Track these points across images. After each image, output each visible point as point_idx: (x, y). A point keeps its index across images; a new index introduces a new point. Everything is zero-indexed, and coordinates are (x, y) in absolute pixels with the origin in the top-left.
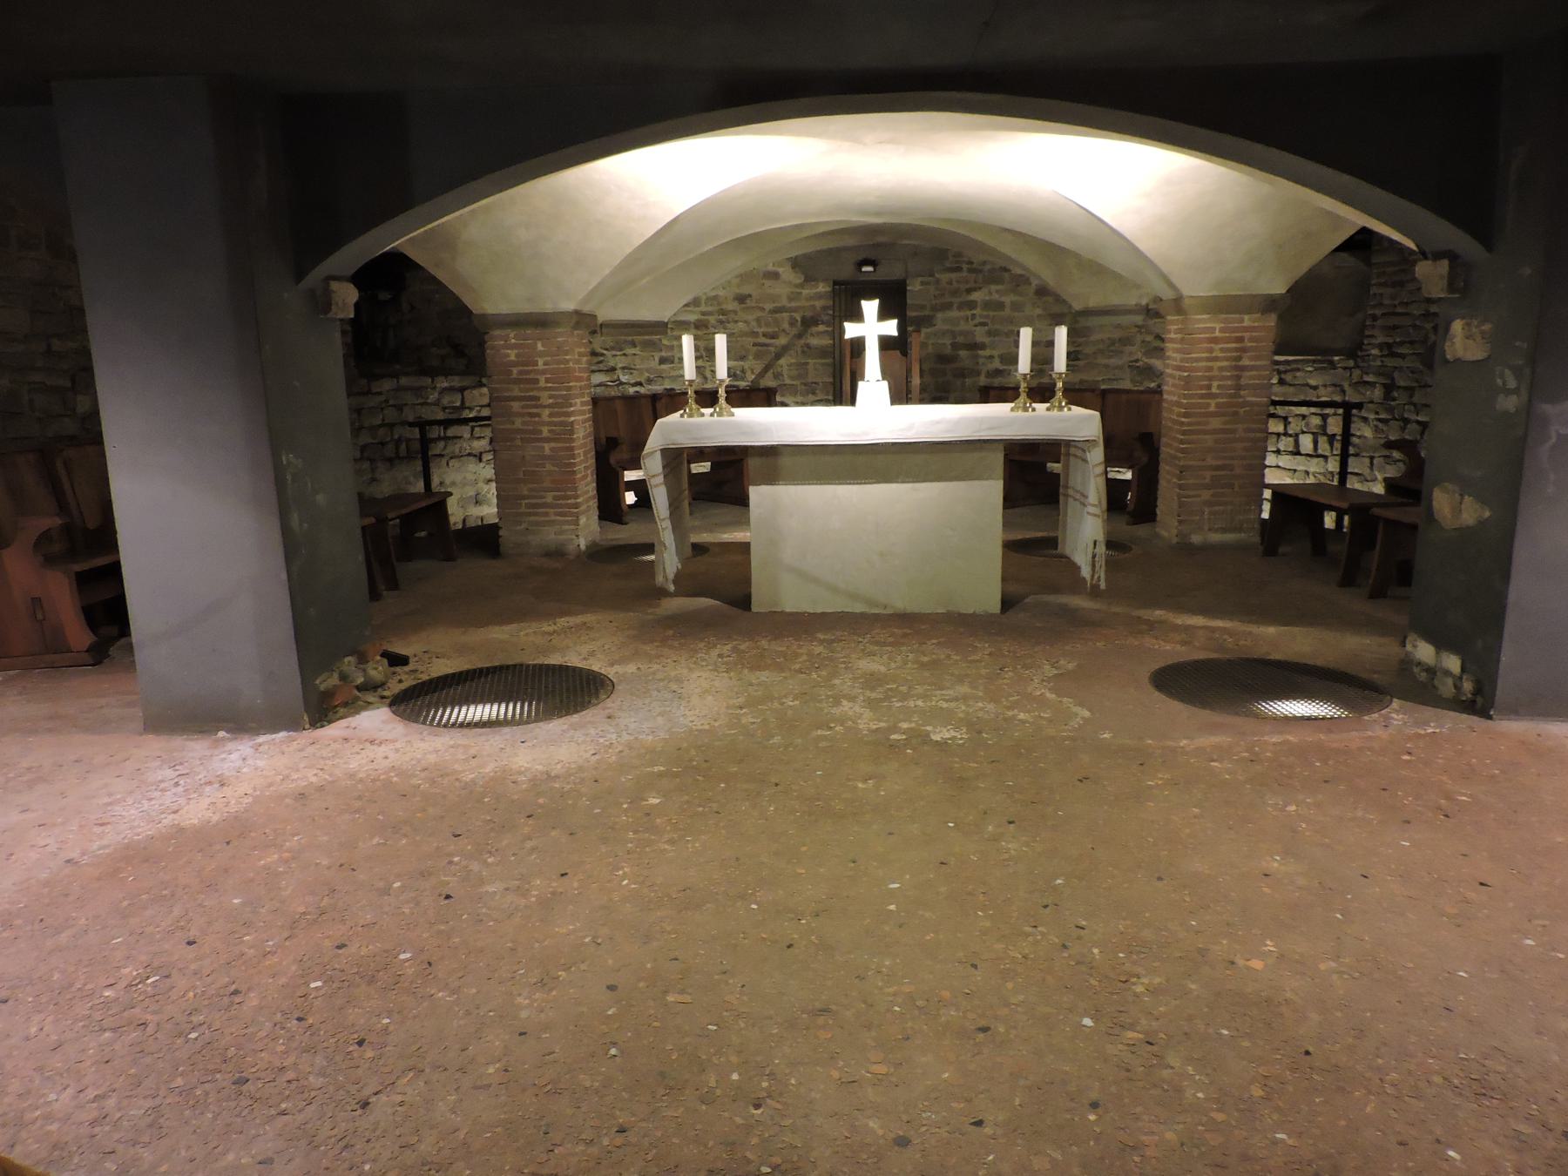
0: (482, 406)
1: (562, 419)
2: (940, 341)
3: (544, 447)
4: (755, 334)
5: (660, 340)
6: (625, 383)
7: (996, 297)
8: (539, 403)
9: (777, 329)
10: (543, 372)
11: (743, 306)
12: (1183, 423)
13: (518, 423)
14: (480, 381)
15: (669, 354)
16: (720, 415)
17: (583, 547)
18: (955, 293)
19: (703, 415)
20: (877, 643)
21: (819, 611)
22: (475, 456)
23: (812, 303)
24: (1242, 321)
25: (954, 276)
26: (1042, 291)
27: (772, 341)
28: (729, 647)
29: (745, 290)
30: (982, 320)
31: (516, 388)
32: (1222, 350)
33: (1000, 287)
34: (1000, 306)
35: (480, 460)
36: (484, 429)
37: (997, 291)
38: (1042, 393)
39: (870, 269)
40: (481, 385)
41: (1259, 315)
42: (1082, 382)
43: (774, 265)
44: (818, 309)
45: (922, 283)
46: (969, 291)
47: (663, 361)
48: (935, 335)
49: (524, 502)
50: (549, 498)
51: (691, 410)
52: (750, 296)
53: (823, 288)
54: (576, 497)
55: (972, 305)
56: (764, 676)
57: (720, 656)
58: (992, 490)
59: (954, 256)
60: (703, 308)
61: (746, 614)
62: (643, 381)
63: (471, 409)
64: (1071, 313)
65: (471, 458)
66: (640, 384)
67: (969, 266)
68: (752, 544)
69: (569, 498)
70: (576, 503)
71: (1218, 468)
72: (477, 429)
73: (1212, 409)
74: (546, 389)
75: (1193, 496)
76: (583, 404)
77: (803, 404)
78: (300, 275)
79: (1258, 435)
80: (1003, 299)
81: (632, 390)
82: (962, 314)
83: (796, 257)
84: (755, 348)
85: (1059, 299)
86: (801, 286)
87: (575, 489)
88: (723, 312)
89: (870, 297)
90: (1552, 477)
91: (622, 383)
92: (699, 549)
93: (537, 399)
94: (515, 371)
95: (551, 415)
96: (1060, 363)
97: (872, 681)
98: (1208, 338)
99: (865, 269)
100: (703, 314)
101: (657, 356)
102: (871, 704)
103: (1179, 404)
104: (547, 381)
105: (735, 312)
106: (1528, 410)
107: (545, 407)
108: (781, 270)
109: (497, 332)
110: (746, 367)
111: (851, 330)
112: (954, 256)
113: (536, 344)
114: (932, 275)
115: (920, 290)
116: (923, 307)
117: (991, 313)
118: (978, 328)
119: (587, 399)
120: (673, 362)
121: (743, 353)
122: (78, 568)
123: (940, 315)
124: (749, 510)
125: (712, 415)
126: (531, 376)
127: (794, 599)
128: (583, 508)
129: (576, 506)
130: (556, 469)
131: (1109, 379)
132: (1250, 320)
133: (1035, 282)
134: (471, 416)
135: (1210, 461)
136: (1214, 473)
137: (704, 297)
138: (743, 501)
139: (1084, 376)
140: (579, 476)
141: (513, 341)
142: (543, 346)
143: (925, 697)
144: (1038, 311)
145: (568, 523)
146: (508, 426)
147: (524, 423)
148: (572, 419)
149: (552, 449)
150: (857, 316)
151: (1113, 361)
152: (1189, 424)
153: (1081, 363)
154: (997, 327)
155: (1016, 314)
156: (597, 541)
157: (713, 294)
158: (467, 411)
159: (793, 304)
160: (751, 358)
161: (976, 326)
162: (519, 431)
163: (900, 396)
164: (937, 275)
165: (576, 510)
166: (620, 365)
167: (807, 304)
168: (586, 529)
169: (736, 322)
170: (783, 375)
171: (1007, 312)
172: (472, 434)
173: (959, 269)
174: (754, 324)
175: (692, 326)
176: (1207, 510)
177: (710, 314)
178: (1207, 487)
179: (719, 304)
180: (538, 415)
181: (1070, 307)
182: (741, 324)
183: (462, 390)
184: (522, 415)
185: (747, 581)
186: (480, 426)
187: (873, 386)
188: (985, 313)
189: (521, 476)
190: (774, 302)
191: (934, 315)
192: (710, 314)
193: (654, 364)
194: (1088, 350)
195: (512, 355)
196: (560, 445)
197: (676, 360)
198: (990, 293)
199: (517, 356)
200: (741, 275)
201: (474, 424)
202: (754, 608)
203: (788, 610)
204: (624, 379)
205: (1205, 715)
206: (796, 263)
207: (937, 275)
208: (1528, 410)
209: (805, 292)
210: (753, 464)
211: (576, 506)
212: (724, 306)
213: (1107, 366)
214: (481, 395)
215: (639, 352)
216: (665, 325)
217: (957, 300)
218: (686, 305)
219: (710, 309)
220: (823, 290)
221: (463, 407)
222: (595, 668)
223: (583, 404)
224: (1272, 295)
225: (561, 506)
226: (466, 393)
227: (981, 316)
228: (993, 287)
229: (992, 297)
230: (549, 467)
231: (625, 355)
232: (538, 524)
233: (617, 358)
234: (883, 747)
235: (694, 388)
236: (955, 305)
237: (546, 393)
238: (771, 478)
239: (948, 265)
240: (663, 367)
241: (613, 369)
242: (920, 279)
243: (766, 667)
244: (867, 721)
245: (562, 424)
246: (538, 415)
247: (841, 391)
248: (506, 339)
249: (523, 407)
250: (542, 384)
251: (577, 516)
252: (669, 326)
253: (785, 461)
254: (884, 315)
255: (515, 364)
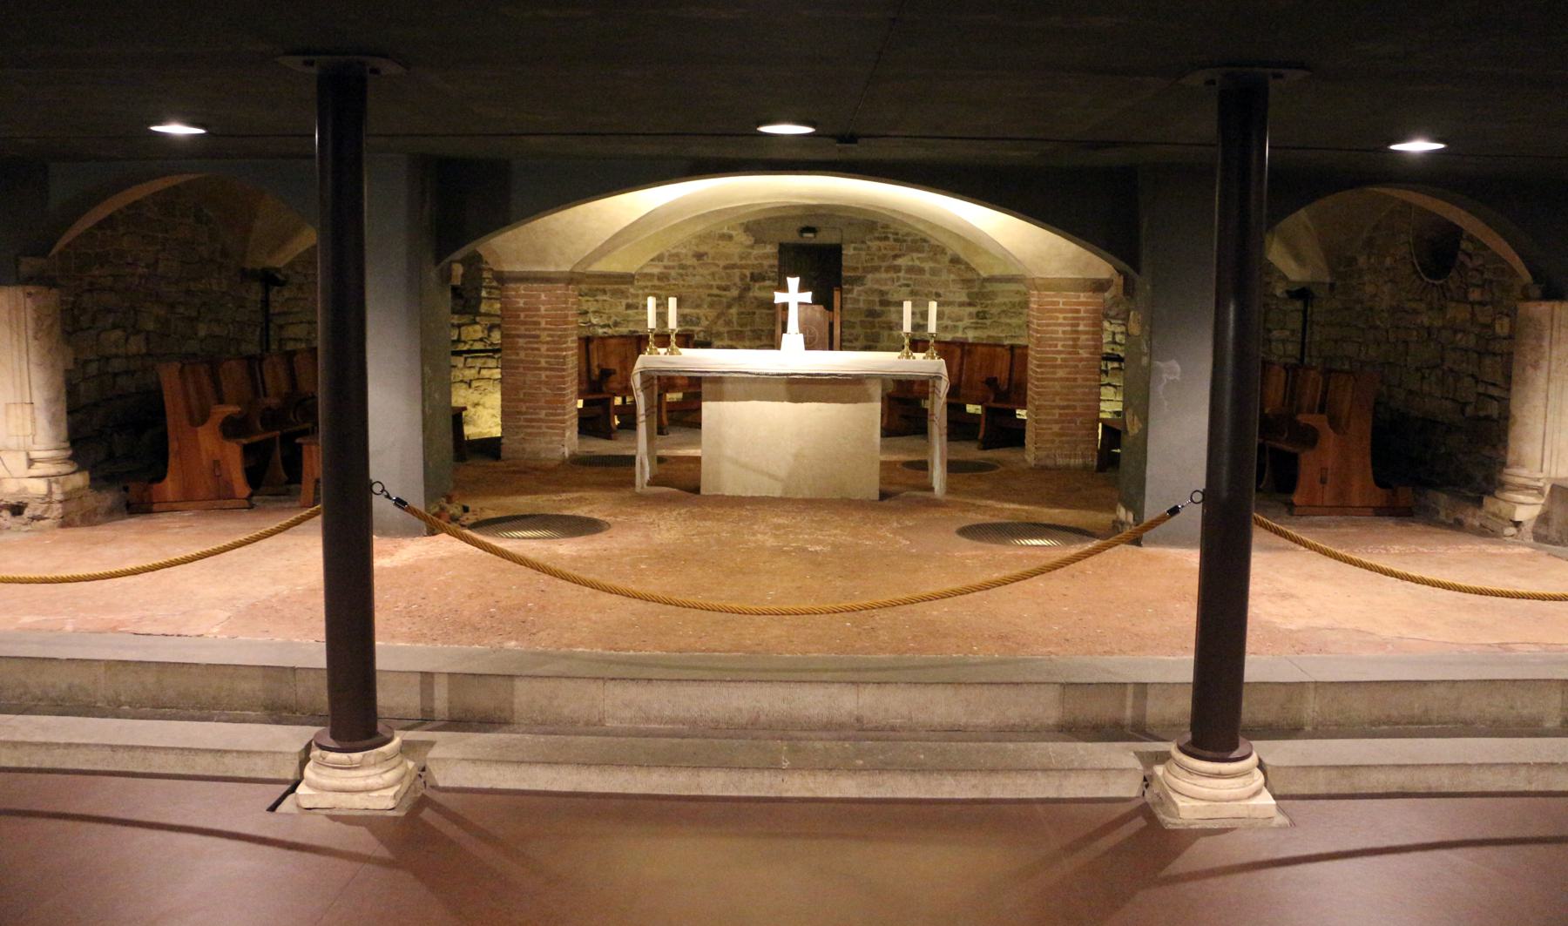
0: (474, 341)
1: (558, 353)
2: (871, 298)
3: (540, 375)
4: (711, 287)
5: (628, 289)
6: (595, 325)
7: (917, 263)
8: (539, 340)
9: (729, 283)
10: (543, 317)
11: (701, 262)
12: (1037, 372)
13: (522, 355)
14: (474, 320)
15: (635, 301)
16: (672, 354)
17: (567, 455)
18: (883, 258)
19: (659, 354)
20: (785, 511)
21: (749, 494)
22: (466, 382)
23: (760, 261)
24: (1079, 297)
25: (882, 244)
26: (955, 260)
27: (724, 293)
28: (685, 510)
29: (703, 249)
30: (905, 282)
31: (523, 328)
32: (1065, 318)
33: (920, 255)
34: (921, 271)
35: (470, 386)
36: (476, 360)
37: (918, 258)
38: (918, 345)
39: (811, 235)
40: (476, 323)
41: (1091, 294)
42: (989, 337)
43: (728, 229)
44: (766, 268)
45: (855, 249)
46: (895, 257)
47: (629, 307)
48: (866, 293)
49: (522, 417)
50: (542, 414)
51: (651, 349)
52: (706, 254)
53: (771, 249)
54: (565, 415)
55: (897, 269)
56: (708, 523)
57: (679, 514)
58: (871, 412)
59: (882, 228)
60: (666, 262)
61: (697, 496)
62: (611, 323)
63: (465, 342)
64: (978, 279)
65: (462, 384)
66: (609, 326)
67: (895, 237)
68: (703, 460)
69: (559, 415)
70: (564, 420)
71: (1064, 408)
72: (469, 360)
73: (1059, 362)
74: (545, 329)
75: (1046, 429)
76: (573, 342)
77: (751, 348)
78: (437, 263)
79: (1093, 383)
80: (923, 265)
81: (600, 331)
82: (889, 275)
83: (748, 222)
84: (709, 299)
85: (969, 268)
86: (752, 247)
87: (564, 408)
88: (683, 267)
89: (793, 275)
90: (1166, 403)
91: (593, 325)
92: (661, 460)
93: (537, 337)
94: (522, 315)
95: (548, 350)
96: (932, 326)
97: (778, 527)
98: (1071, 309)
99: (806, 235)
100: (665, 267)
101: (624, 302)
102: (776, 536)
103: (1036, 358)
104: (547, 323)
105: (694, 268)
106: (1150, 364)
107: (544, 343)
108: (734, 233)
109: (512, 285)
110: (701, 314)
111: (779, 297)
112: (882, 228)
113: (540, 295)
114: (863, 242)
115: (853, 255)
116: (855, 269)
117: (913, 276)
118: (903, 288)
119: (575, 338)
120: (637, 308)
121: (699, 302)
122: (245, 441)
123: (870, 276)
124: (700, 434)
125: (666, 354)
126: (535, 319)
127: (729, 490)
128: (569, 423)
129: (563, 422)
130: (550, 392)
131: (1012, 336)
132: (1084, 296)
133: (949, 252)
134: (465, 348)
135: (1058, 402)
136: (1062, 411)
137: (667, 254)
138: (697, 425)
139: (992, 333)
140: (567, 398)
141: (523, 292)
142: (546, 296)
143: (810, 534)
144: (952, 276)
145: (557, 435)
146: (513, 357)
147: (527, 355)
148: (564, 353)
149: (547, 377)
150: (783, 288)
151: (1014, 321)
152: (1042, 373)
153: (988, 322)
154: (917, 288)
155: (935, 278)
156: (577, 452)
157: (674, 251)
158: (463, 344)
159: (743, 262)
160: (706, 306)
161: (900, 286)
162: (522, 361)
163: (810, 345)
164: (869, 243)
165: (563, 425)
166: (592, 309)
167: (756, 262)
168: (569, 442)
169: (694, 275)
170: (733, 323)
171: (927, 276)
172: (465, 364)
173: (886, 238)
174: (709, 277)
175: (656, 278)
176: (570, 305)
177: (673, 268)
178: (1056, 422)
179: (680, 260)
180: (538, 349)
181: (979, 274)
182: (697, 277)
183: (459, 326)
184: (526, 349)
185: (699, 479)
186: (472, 357)
187: (793, 338)
188: (909, 276)
189: (522, 396)
190: (727, 260)
191: (865, 277)
192: (673, 268)
193: (621, 308)
194: (994, 311)
195: (521, 303)
196: (553, 373)
197: (641, 306)
198: (913, 260)
199: (524, 303)
200: (700, 236)
201: (467, 355)
202: (703, 492)
203: (727, 494)
204: (594, 321)
205: (976, 543)
206: (748, 228)
207: (869, 243)
208: (1150, 364)
209: (755, 252)
210: (705, 387)
211: (563, 422)
212: (684, 262)
213: (1009, 325)
214: (475, 331)
215: (608, 299)
216: (633, 276)
217: (884, 264)
218: (652, 260)
219: (671, 264)
220: (772, 251)
221: (459, 341)
222: (596, 517)
223: (573, 342)
224: (1099, 280)
225: (553, 421)
226: (463, 328)
227: (904, 279)
228: (915, 255)
229: (915, 264)
230: (544, 390)
231: (597, 301)
232: (530, 434)
233: (590, 303)
234: (779, 552)
235: (675, 333)
236: (883, 269)
237: (546, 333)
238: (719, 397)
239: (877, 235)
240: (630, 312)
241: (586, 313)
242: (853, 245)
243: (710, 519)
244: (771, 542)
245: (557, 357)
246: (538, 349)
247: (771, 341)
248: (516, 290)
249: (526, 343)
250: (543, 325)
251: (564, 429)
252: (636, 277)
253: (728, 387)
254: (802, 289)
255: (523, 310)
